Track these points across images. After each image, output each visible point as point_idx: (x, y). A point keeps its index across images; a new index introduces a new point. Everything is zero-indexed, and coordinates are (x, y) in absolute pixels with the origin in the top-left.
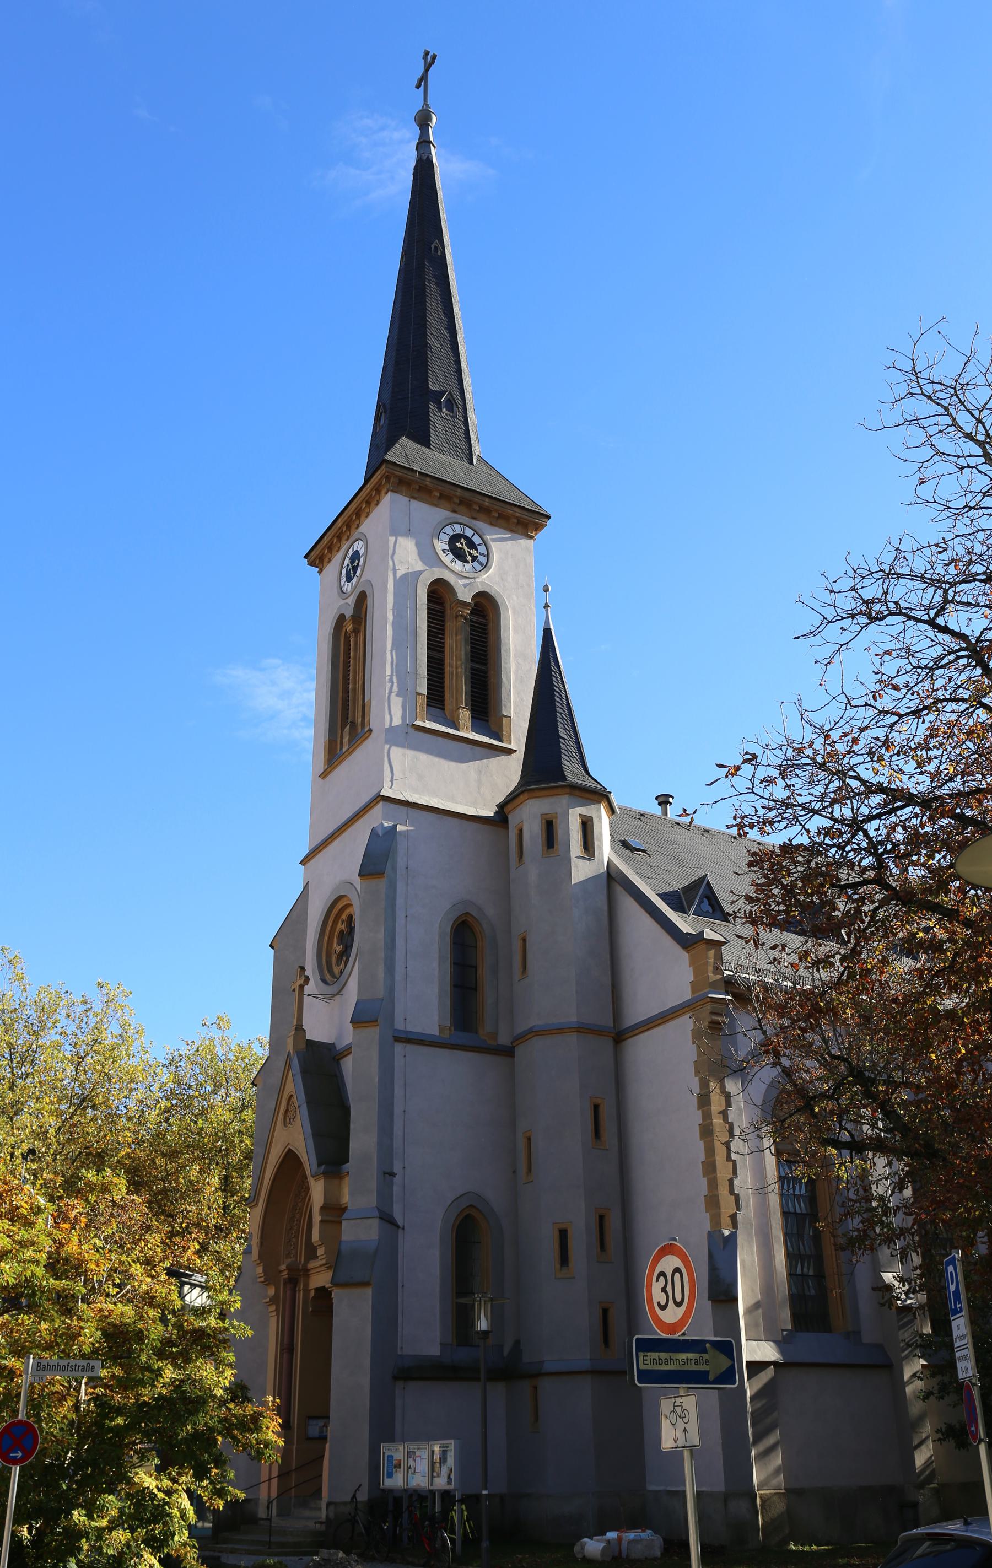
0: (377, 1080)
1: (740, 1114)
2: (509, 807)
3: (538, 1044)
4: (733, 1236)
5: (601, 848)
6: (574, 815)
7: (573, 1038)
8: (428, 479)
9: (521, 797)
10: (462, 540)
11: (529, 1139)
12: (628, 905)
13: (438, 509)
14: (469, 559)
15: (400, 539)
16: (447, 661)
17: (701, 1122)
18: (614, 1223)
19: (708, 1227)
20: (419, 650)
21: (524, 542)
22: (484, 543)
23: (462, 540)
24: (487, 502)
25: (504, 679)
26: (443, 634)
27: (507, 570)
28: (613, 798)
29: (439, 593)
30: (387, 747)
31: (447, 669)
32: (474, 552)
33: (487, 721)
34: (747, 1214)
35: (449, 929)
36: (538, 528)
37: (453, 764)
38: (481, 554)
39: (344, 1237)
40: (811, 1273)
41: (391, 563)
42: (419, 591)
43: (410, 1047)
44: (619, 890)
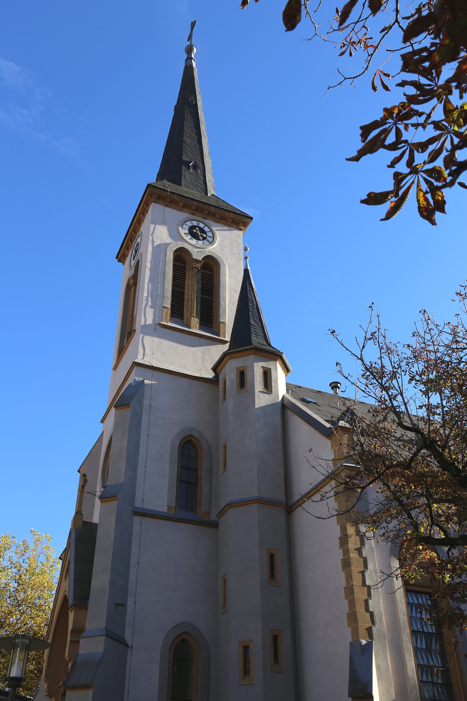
0: (113, 536)
1: (372, 551)
2: (219, 368)
3: (231, 512)
4: (369, 646)
5: (277, 387)
6: (258, 368)
7: (254, 508)
8: (176, 196)
9: (225, 359)
10: (197, 228)
11: (225, 581)
12: (296, 422)
13: (183, 213)
14: (201, 238)
15: (157, 226)
16: (186, 292)
17: (342, 558)
18: (285, 642)
19: (350, 639)
20: (166, 284)
21: (237, 232)
22: (211, 231)
23: (197, 228)
24: (212, 209)
25: (222, 302)
26: (185, 279)
27: (226, 246)
28: (284, 356)
29: (181, 256)
30: (142, 335)
31: (186, 296)
32: (205, 235)
33: (212, 327)
34: (382, 626)
35: (178, 444)
36: (245, 225)
37: (186, 348)
38: (209, 236)
39: (81, 652)
40: (440, 681)
41: (151, 238)
42: (168, 253)
43: (144, 519)
44: (289, 413)
